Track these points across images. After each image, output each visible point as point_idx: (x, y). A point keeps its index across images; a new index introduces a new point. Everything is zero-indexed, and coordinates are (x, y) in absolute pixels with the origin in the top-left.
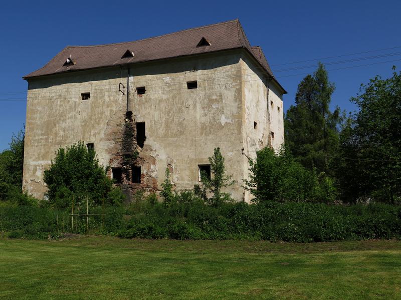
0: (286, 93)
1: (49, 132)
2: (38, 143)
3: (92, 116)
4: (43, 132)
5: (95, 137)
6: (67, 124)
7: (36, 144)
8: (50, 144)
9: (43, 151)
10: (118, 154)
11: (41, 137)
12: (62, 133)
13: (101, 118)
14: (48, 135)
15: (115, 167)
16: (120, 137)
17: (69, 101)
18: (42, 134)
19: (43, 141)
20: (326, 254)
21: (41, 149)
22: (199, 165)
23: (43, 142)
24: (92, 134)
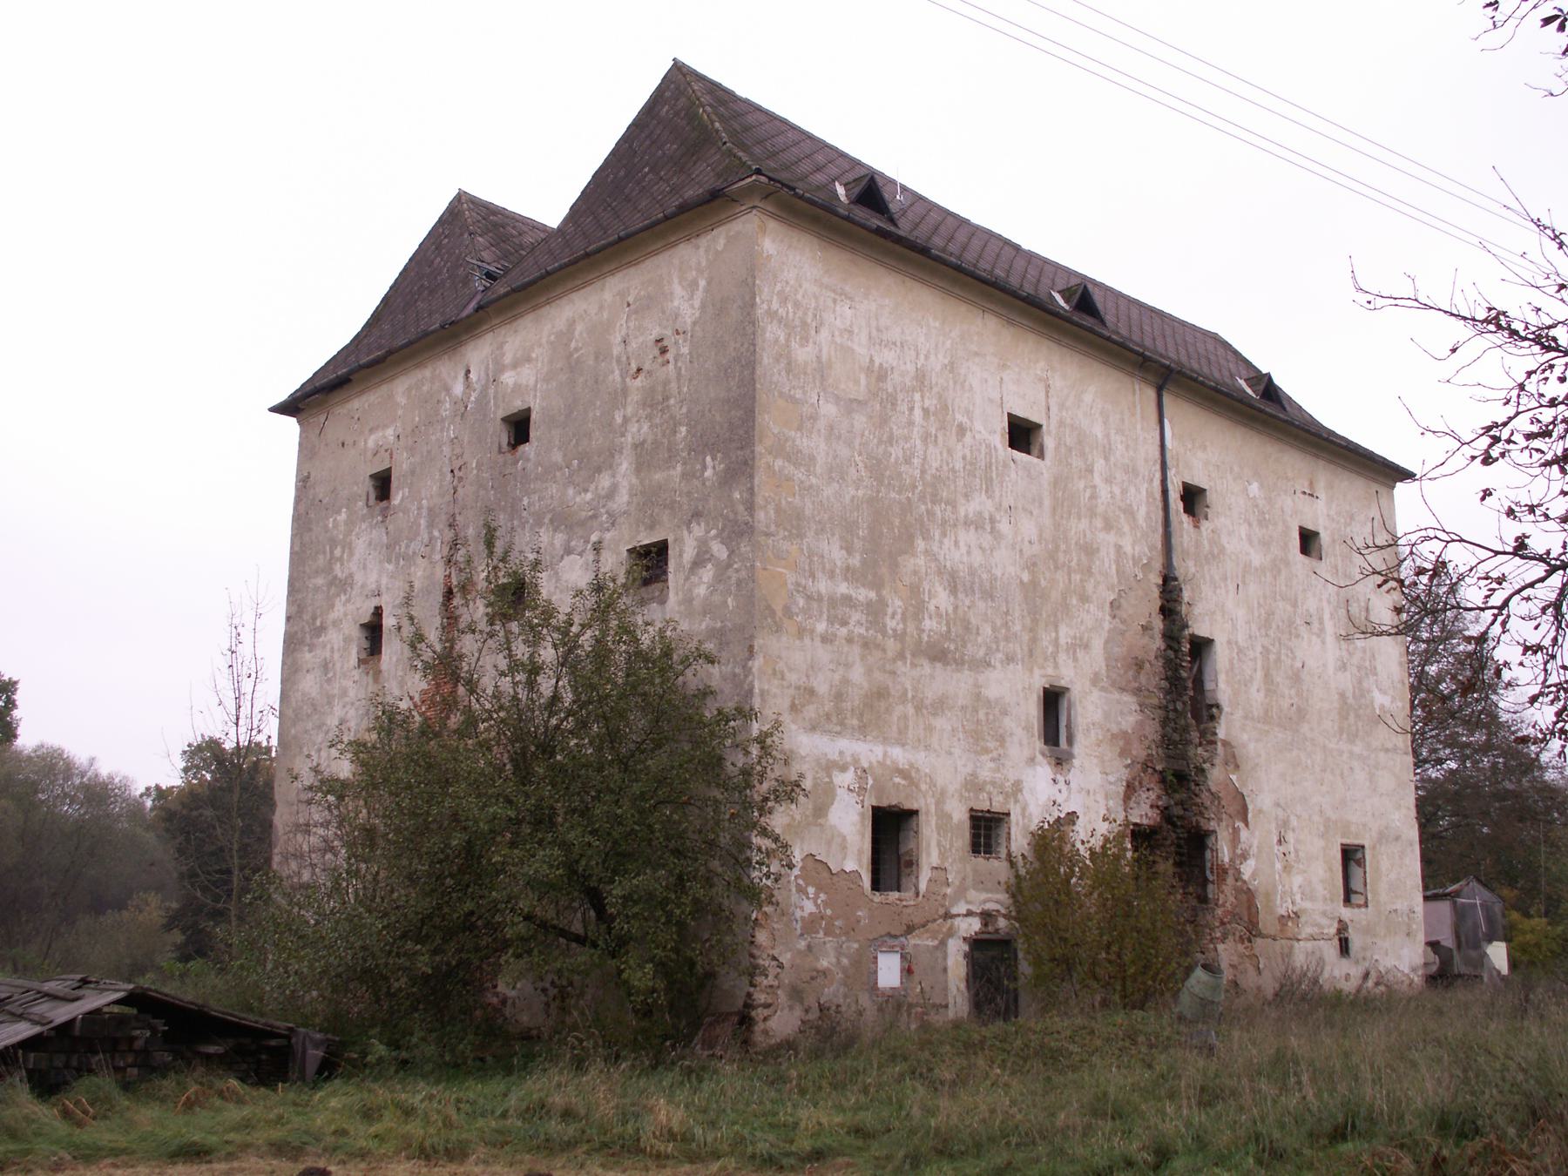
0: (1406, 475)
1: (884, 570)
2: (831, 621)
3: (1057, 548)
4: (856, 561)
5: (1075, 660)
6: (961, 549)
7: (821, 627)
8: (892, 645)
9: (857, 674)
10: (1146, 765)
11: (843, 588)
12: (941, 599)
13: (1089, 571)
14: (877, 585)
15: (1145, 821)
16: (1152, 677)
17: (961, 431)
18: (849, 574)
19: (856, 616)
20: (560, 819)
21: (848, 666)
22: (529, 410)
23: (857, 623)
24: (1062, 641)
